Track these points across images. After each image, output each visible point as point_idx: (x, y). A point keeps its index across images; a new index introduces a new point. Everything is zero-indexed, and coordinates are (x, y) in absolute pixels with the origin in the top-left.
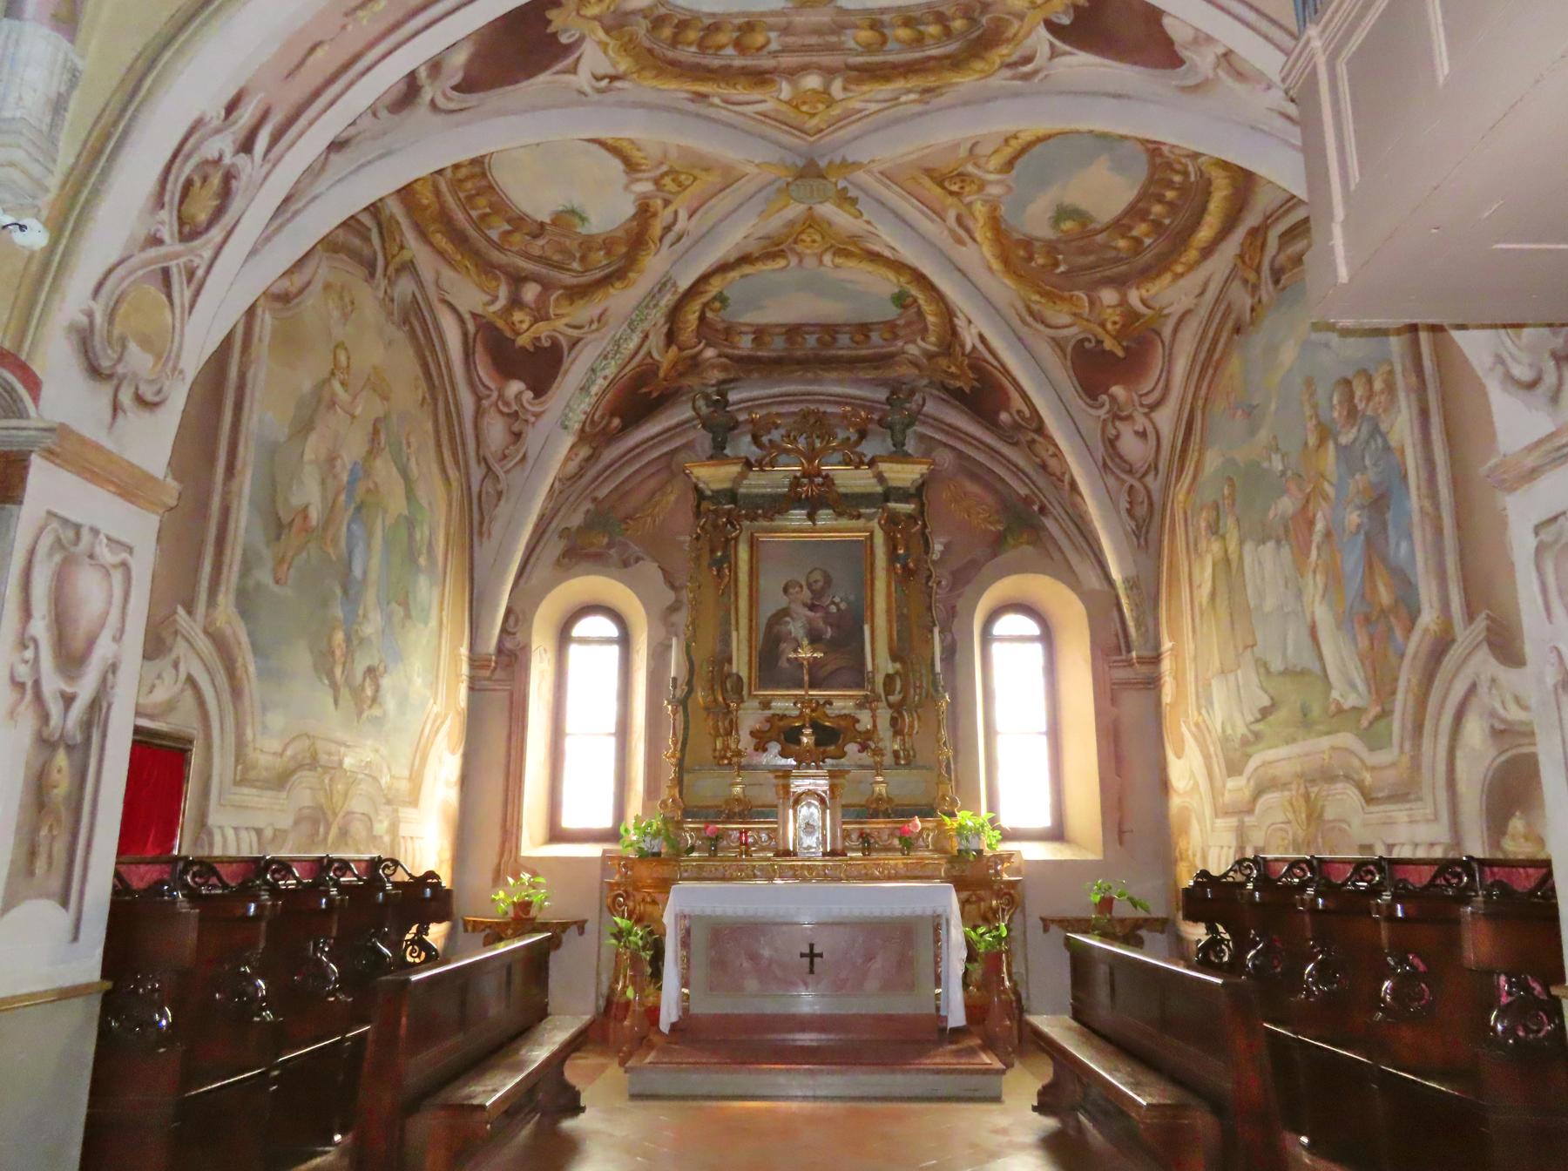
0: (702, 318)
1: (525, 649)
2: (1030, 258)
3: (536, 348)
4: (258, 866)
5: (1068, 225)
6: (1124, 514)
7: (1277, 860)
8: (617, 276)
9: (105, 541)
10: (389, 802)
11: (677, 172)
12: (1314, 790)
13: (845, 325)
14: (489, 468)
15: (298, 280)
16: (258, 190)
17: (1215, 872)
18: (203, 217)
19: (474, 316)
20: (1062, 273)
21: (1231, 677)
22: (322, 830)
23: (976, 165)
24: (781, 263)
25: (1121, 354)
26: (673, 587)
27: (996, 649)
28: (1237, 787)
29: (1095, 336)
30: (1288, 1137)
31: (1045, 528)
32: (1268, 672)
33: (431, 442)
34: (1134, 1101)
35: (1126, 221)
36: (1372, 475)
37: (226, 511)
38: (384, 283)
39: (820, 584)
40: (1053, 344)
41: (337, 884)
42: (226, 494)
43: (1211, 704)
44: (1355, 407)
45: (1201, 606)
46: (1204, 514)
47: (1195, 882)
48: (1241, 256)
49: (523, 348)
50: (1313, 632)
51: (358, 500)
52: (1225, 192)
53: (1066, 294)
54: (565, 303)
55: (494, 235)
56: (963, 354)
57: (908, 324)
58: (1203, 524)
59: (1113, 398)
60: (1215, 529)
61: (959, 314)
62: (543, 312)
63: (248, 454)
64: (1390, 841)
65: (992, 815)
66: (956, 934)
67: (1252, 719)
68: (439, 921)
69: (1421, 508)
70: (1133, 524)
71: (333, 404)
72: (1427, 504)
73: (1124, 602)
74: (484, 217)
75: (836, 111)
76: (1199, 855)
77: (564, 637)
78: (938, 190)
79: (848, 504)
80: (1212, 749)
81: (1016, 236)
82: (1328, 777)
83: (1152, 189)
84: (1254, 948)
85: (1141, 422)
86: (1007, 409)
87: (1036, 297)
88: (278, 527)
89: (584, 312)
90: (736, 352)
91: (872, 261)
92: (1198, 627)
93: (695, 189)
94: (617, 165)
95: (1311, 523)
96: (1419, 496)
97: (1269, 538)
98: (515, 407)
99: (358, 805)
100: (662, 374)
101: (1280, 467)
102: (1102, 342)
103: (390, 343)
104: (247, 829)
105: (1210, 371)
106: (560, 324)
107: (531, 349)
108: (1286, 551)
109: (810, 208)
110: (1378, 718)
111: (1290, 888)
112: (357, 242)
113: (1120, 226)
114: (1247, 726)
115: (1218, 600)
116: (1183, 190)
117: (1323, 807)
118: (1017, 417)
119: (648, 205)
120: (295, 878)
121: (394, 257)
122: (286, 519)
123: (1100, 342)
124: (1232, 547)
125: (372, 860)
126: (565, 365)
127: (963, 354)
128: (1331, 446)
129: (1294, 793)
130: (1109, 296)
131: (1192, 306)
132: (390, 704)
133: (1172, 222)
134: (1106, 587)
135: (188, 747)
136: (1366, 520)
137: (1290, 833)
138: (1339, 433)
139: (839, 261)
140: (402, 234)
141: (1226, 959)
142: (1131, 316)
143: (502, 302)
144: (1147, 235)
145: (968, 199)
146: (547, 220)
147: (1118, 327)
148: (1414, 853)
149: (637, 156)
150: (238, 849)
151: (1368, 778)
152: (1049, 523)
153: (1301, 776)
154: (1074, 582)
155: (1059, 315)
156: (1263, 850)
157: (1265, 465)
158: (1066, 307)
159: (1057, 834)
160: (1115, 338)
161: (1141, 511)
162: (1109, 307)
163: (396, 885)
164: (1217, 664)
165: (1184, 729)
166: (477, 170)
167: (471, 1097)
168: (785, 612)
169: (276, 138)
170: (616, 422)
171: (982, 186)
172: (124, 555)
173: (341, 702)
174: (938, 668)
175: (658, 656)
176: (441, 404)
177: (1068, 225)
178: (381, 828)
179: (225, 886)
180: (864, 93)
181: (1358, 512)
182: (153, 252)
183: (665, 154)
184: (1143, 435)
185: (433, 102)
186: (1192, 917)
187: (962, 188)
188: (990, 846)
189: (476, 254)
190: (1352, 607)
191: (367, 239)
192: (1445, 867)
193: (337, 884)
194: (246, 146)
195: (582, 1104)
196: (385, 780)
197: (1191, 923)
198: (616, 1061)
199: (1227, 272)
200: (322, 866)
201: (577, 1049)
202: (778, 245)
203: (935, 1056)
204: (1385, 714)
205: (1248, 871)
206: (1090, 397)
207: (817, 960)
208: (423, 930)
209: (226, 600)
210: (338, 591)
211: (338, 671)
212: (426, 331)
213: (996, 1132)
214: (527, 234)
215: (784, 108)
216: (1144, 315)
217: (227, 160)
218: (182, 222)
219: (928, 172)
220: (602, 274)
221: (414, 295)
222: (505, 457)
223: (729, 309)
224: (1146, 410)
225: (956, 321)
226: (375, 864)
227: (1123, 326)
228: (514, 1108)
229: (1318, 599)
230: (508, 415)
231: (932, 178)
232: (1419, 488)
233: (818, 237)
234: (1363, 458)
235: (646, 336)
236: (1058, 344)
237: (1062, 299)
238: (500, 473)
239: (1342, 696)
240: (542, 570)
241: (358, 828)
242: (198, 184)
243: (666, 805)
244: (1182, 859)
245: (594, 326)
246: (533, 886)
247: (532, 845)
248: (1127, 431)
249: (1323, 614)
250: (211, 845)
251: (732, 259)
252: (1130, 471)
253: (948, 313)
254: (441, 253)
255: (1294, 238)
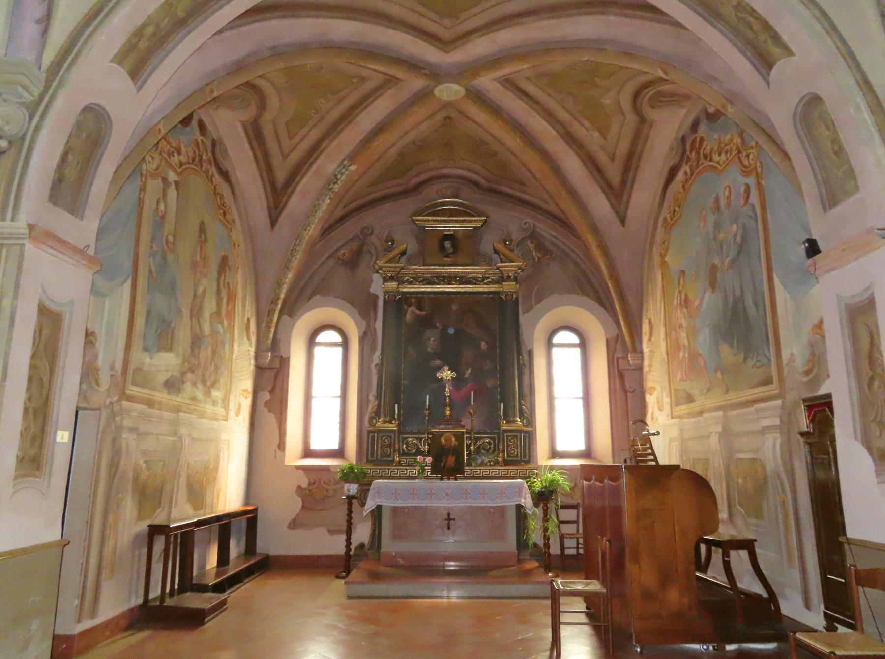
77: (311, 343)
207: (452, 522)
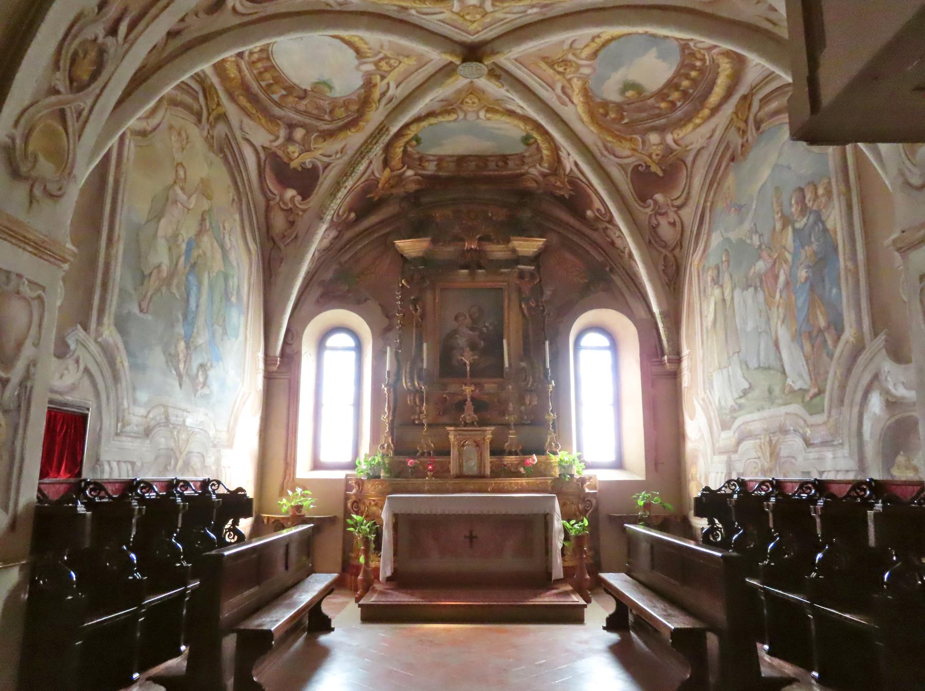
0: (405, 151)
1: (298, 353)
2: (606, 114)
3: (303, 168)
4: (130, 486)
5: (630, 93)
6: (661, 273)
7: (751, 481)
8: (353, 123)
9: (26, 282)
10: (215, 446)
11: (389, 58)
12: (775, 439)
13: (491, 156)
14: (274, 242)
15: (154, 121)
16: (122, 61)
17: (713, 488)
18: (86, 77)
19: (264, 148)
20: (626, 123)
21: (725, 371)
22: (173, 462)
23: (574, 54)
24: (454, 116)
25: (660, 174)
26: (387, 316)
27: (582, 354)
28: (727, 438)
29: (645, 163)
30: (759, 645)
31: (612, 281)
32: (747, 366)
33: (238, 229)
34: (666, 626)
35: (665, 91)
36: (815, 246)
37: (107, 265)
38: (207, 127)
39: (477, 315)
40: (619, 168)
41: (182, 495)
42: (108, 255)
43: (713, 387)
44: (806, 205)
45: (707, 328)
46: (710, 272)
47: (702, 494)
48: (736, 113)
49: (295, 169)
50: (777, 345)
51: (192, 261)
52: (727, 72)
53: (629, 137)
54: (321, 140)
55: (276, 97)
56: (564, 174)
57: (531, 156)
58: (709, 279)
59: (656, 202)
60: (716, 281)
61: (562, 149)
62: (306, 146)
63: (121, 231)
64: (822, 470)
65: (579, 454)
66: (558, 523)
67: (737, 396)
68: (246, 517)
69: (846, 266)
70: (666, 279)
71: (175, 202)
72: (850, 265)
73: (660, 325)
74: (269, 85)
75: (488, 20)
76: (703, 478)
78: (550, 71)
79: (496, 265)
80: (712, 415)
81: (599, 100)
82: (784, 431)
83: (682, 71)
84: (737, 533)
85: (672, 216)
86: (591, 209)
87: (609, 139)
88: (142, 278)
89: (332, 146)
90: (426, 172)
91: (509, 115)
92: (705, 342)
93: (402, 68)
94: (351, 53)
95: (776, 277)
96: (844, 259)
97: (750, 286)
98: (290, 206)
99: (194, 447)
100: (380, 185)
101: (758, 243)
102: (650, 166)
103: (211, 163)
104: (125, 462)
105: (715, 185)
106: (317, 154)
107: (300, 169)
108: (761, 296)
109: (472, 82)
110: (815, 395)
111: (759, 497)
112: (188, 100)
113: (661, 94)
114: (734, 400)
115: (718, 324)
116: (701, 71)
117: (780, 449)
118: (597, 214)
119: (371, 79)
120: (155, 492)
121: (213, 110)
122: (147, 273)
123: (648, 167)
124: (727, 292)
125: (171, 481)
126: (321, 179)
127: (564, 174)
128: (790, 229)
129: (763, 441)
130: (654, 138)
131: (705, 145)
132: (215, 386)
133: (693, 92)
134: (650, 316)
135: (87, 412)
136: (811, 274)
137: (760, 464)
138: (796, 221)
139: (489, 115)
140: (218, 97)
141: (719, 539)
142: (669, 151)
143: (281, 141)
144: (679, 100)
145: (569, 77)
146: (309, 89)
147: (660, 157)
148: (836, 477)
149: (363, 47)
150: (120, 475)
151: (809, 432)
152: (615, 278)
153: (766, 430)
154: (630, 315)
155: (624, 149)
156: (743, 474)
157: (748, 241)
158: (628, 145)
159: (619, 465)
160: (658, 164)
161: (672, 270)
162: (654, 145)
163: (218, 496)
164: (717, 364)
165: (696, 403)
166: (264, 55)
167: (261, 625)
168: (455, 332)
169: (132, 27)
170: (353, 215)
171: (579, 66)
172: (40, 292)
173: (183, 386)
174: (548, 366)
175: (379, 356)
176: (244, 207)
177: (630, 93)
178: (210, 460)
179: (110, 497)
180: (504, 8)
181: (806, 270)
182: (53, 99)
183: (382, 47)
184: (673, 224)
185: (234, 9)
186: (699, 514)
187: (565, 69)
188: (578, 472)
189: (265, 111)
190: (801, 327)
191: (196, 99)
192: (857, 485)
193: (182, 495)
194: (113, 31)
195: (332, 626)
196: (212, 433)
197: (699, 518)
198: (353, 600)
199: (727, 123)
200: (171, 485)
201: (329, 593)
202: (452, 105)
203: (544, 597)
204: (821, 392)
205: (734, 487)
206: (640, 199)
208: (236, 523)
209: (108, 320)
210: (181, 317)
211: (181, 366)
212: (236, 161)
213: (580, 642)
214: (296, 97)
215: (455, 17)
216: (676, 150)
217: (100, 40)
218: (71, 81)
219: (544, 59)
220: (342, 123)
221: (226, 135)
222: (284, 236)
223: (421, 145)
224: (675, 209)
225: (561, 153)
226: (205, 484)
227: (663, 157)
228: (293, 628)
229: (779, 323)
230: (286, 210)
231: (547, 63)
232: (844, 254)
233: (476, 100)
234: (810, 236)
235: (371, 162)
236: (622, 167)
237: (626, 140)
238: (282, 246)
239: (793, 382)
240: (307, 306)
241: (195, 461)
242: (81, 55)
243: (384, 448)
244: (692, 480)
245: (339, 156)
246: (303, 496)
247: (303, 470)
248: (663, 221)
249: (784, 334)
250: (102, 472)
251: (423, 114)
252: (665, 246)
253: (555, 149)
254: (243, 109)
255: (769, 101)
